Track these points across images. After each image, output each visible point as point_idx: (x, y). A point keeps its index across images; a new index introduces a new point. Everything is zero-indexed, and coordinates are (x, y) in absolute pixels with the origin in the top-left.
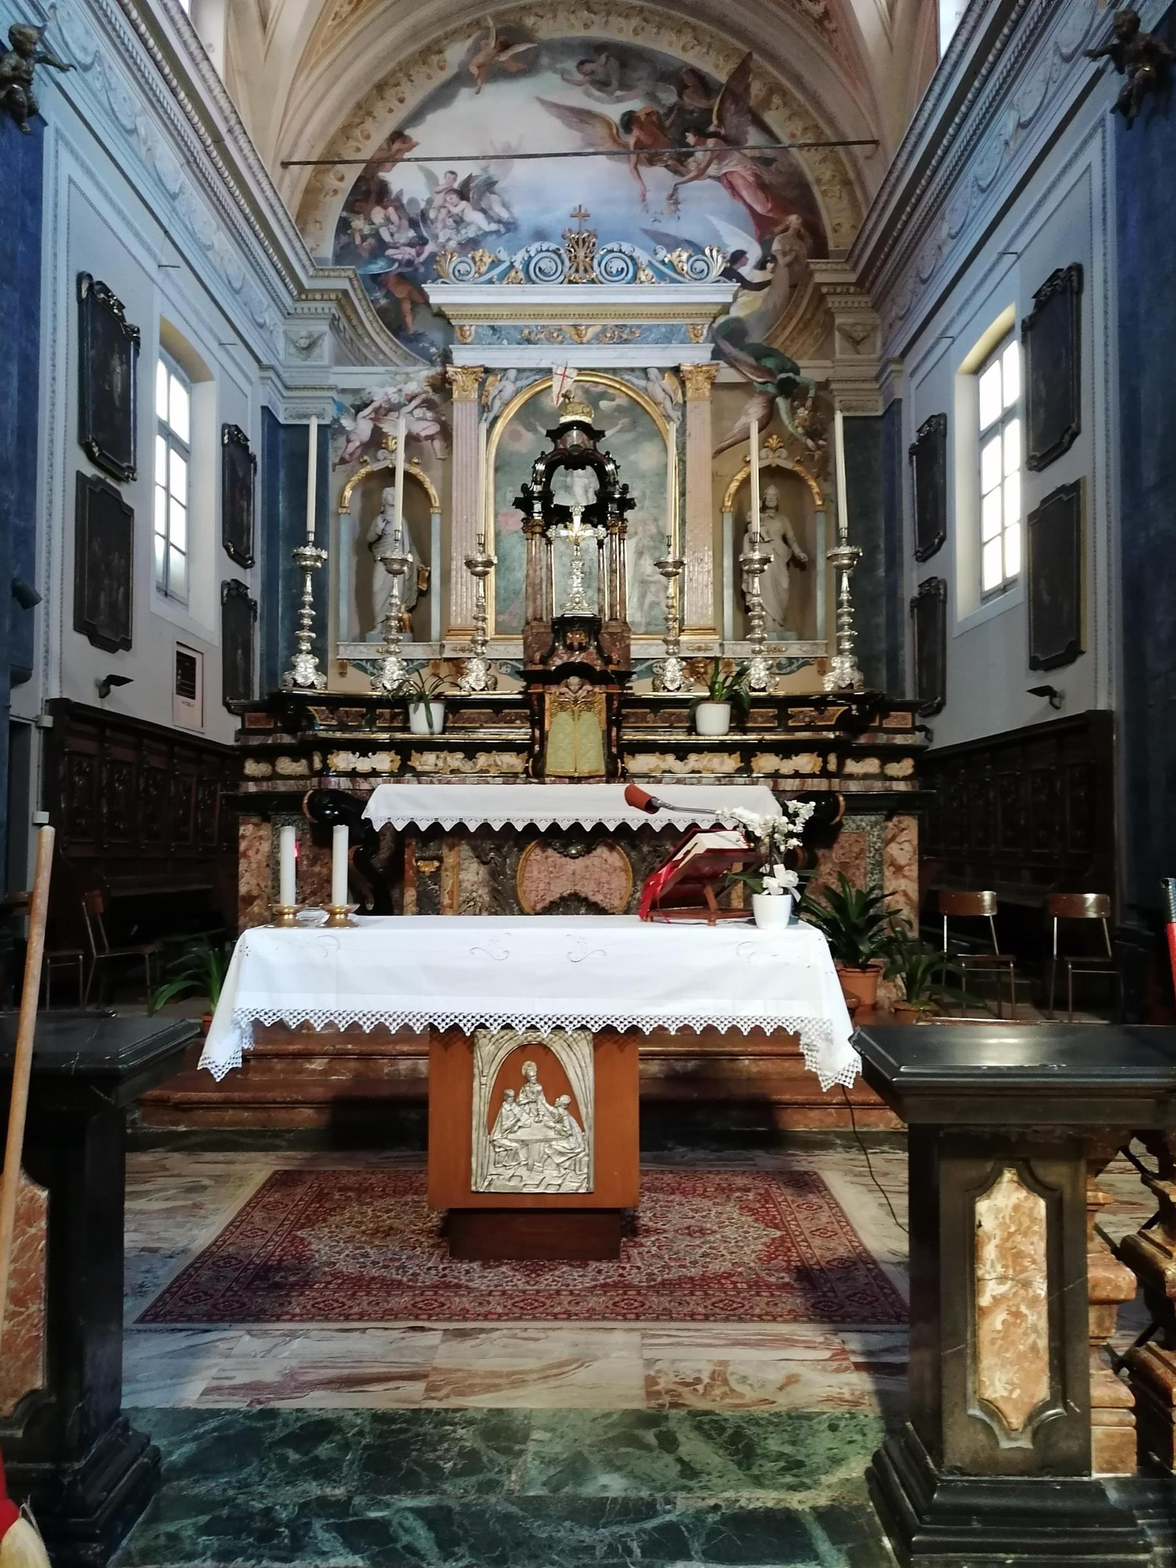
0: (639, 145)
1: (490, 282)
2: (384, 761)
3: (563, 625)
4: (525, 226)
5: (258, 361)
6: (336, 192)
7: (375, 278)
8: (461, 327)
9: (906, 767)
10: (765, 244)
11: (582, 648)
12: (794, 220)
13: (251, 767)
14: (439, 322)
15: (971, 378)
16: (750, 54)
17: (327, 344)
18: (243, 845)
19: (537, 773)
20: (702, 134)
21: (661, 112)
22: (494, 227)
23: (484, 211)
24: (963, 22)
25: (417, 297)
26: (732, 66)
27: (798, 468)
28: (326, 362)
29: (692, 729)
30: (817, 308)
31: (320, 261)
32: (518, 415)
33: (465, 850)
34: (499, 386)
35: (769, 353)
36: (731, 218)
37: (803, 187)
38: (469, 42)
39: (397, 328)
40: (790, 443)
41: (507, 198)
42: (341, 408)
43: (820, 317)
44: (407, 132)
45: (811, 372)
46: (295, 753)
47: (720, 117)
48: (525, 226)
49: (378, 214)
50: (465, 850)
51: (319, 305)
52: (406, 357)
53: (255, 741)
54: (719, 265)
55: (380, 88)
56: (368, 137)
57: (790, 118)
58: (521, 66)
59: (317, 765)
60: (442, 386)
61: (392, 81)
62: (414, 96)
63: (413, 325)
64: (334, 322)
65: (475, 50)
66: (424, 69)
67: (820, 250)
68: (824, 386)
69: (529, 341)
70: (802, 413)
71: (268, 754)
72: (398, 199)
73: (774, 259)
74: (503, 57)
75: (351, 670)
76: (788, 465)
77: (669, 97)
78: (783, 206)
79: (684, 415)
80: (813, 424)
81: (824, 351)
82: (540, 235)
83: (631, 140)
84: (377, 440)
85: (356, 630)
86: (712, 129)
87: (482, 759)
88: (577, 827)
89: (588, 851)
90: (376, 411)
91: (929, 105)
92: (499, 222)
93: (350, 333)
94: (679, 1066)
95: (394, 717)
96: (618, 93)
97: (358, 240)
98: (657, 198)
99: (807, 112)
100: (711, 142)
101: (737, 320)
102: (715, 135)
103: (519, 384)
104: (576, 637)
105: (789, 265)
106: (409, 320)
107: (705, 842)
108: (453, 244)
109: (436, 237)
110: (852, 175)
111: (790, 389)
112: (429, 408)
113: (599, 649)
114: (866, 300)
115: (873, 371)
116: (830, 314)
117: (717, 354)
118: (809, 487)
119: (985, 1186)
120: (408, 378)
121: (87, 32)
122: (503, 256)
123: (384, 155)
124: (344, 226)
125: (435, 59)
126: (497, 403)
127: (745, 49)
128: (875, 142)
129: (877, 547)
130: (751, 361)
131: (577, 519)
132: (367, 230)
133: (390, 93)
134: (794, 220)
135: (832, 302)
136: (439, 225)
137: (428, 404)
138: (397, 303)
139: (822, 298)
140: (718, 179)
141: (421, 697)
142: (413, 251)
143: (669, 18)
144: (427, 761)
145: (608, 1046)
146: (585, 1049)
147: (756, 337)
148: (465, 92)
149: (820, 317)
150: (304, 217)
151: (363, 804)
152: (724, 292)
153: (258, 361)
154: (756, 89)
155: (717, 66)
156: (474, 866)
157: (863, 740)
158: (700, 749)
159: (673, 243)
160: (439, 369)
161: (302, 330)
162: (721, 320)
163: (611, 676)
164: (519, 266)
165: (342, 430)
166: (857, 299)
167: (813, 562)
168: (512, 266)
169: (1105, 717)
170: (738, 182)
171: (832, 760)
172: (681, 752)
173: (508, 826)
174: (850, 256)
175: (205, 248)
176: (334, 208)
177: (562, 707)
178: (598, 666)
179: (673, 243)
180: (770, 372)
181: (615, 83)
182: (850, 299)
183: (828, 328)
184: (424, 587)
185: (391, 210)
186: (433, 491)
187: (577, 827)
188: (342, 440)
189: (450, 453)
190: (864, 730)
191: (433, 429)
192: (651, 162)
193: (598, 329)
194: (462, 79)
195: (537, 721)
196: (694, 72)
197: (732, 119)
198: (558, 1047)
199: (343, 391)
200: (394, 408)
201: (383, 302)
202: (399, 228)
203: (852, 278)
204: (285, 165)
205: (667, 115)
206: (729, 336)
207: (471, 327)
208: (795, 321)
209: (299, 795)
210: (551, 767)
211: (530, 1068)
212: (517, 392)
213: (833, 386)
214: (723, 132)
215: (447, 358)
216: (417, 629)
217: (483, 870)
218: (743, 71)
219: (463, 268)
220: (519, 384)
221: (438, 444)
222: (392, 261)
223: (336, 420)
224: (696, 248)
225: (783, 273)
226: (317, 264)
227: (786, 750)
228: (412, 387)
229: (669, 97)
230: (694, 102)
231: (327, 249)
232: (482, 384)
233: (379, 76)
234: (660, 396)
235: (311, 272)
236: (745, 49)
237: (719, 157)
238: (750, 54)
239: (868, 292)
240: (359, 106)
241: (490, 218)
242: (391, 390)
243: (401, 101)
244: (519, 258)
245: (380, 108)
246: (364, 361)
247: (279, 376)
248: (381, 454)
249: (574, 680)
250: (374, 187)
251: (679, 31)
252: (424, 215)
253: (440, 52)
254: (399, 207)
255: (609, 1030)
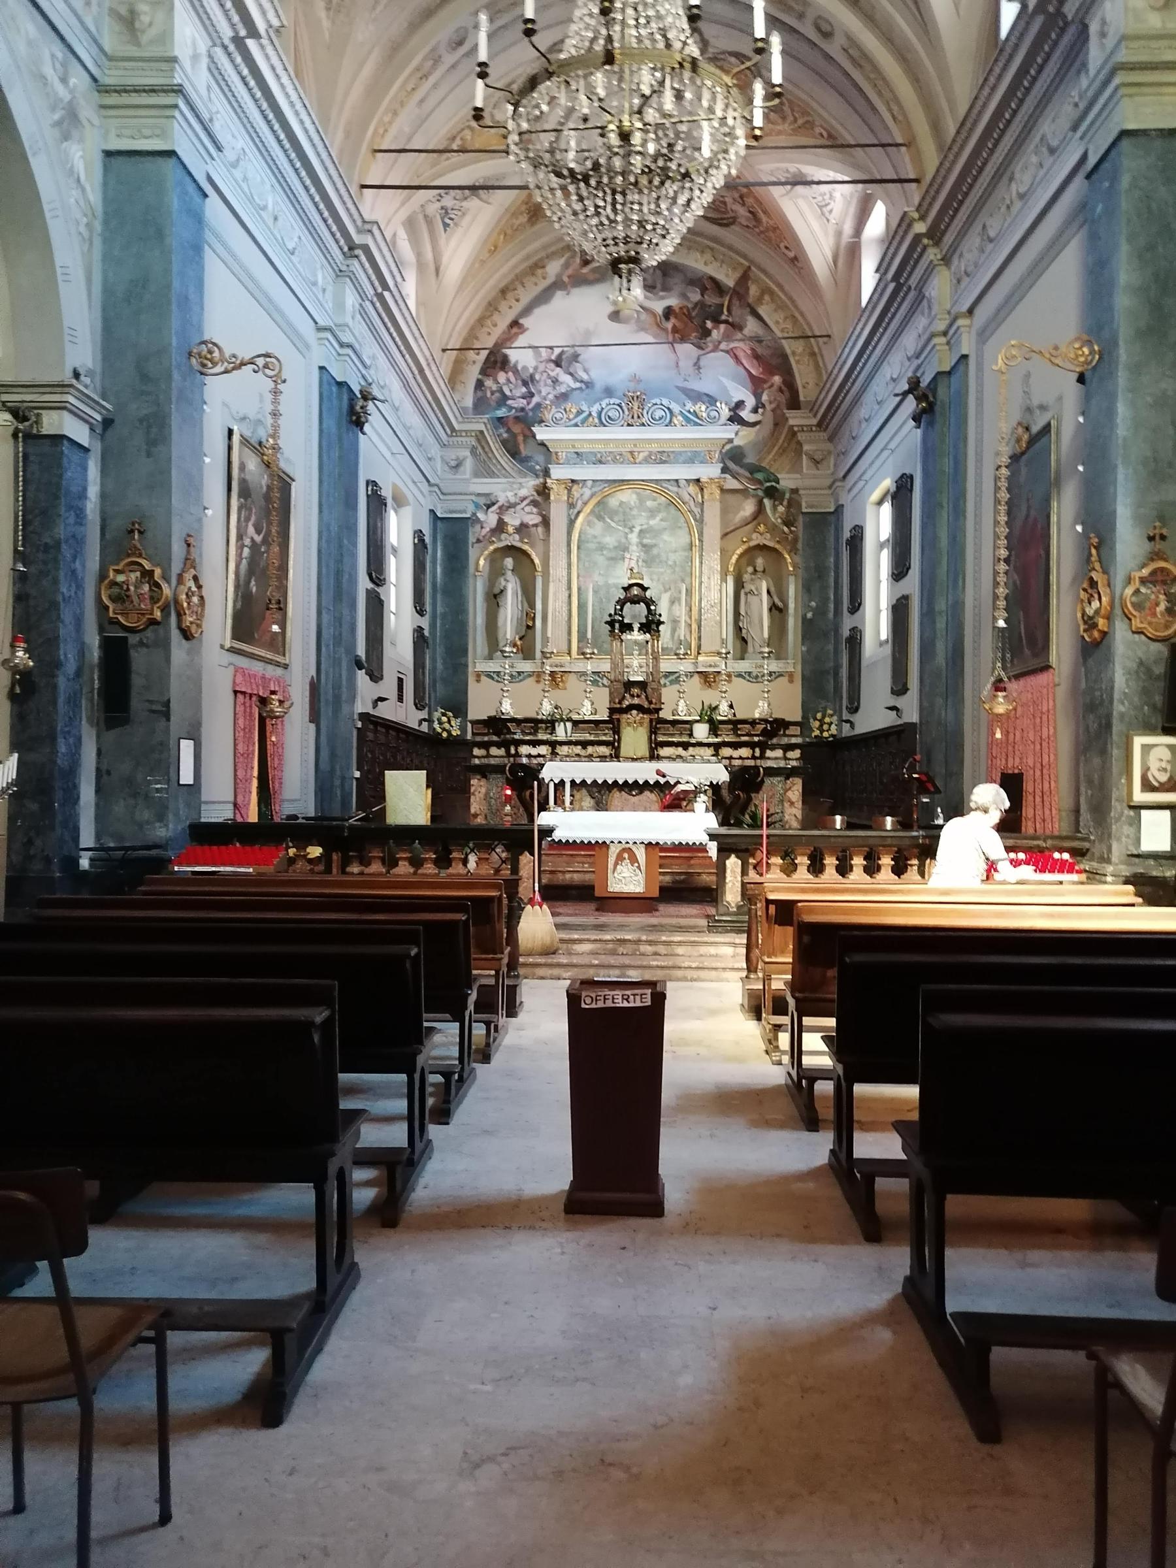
0: (675, 330)
1: (576, 425)
2: (543, 750)
3: (629, 685)
4: (599, 386)
5: (428, 481)
6: (474, 362)
7: (500, 419)
8: (556, 453)
9: (797, 753)
10: (757, 395)
11: (638, 696)
12: (777, 379)
13: (476, 751)
14: (541, 448)
15: (875, 507)
16: (749, 268)
17: (469, 464)
18: (472, 789)
19: (616, 756)
20: (717, 321)
21: (690, 306)
22: (578, 385)
23: (571, 374)
24: (875, 290)
25: (528, 433)
26: (737, 275)
27: (777, 546)
28: (468, 476)
29: (691, 735)
30: (791, 440)
31: (465, 409)
32: (592, 511)
33: (584, 791)
34: (581, 491)
35: (759, 469)
36: (735, 379)
37: (784, 357)
38: (562, 261)
39: (514, 453)
40: (772, 529)
41: (587, 366)
42: (477, 506)
43: (793, 445)
44: (521, 321)
45: (787, 481)
46: (498, 745)
47: (729, 310)
48: (599, 386)
49: (502, 377)
50: (584, 791)
51: (463, 439)
52: (520, 472)
53: (478, 739)
54: (725, 412)
55: (504, 292)
56: (495, 325)
57: (775, 310)
58: (597, 276)
59: (513, 751)
60: (543, 491)
61: (511, 287)
62: (526, 297)
63: (524, 451)
64: (473, 451)
65: (566, 266)
66: (533, 279)
67: (794, 403)
68: (795, 491)
69: (601, 462)
70: (781, 509)
71: (486, 746)
72: (515, 366)
73: (763, 406)
74: (585, 270)
75: (483, 678)
76: (771, 544)
77: (695, 296)
78: (770, 370)
79: (702, 511)
80: (787, 516)
81: (796, 468)
82: (609, 392)
83: (669, 325)
84: (501, 527)
85: (486, 652)
86: (723, 317)
87: (590, 749)
88: (636, 782)
89: (641, 793)
90: (500, 508)
91: (847, 350)
92: (582, 382)
93: (483, 456)
94: (677, 878)
95: (547, 728)
96: (661, 294)
97: (489, 394)
98: (686, 365)
99: (787, 306)
100: (722, 327)
101: (739, 447)
102: (726, 322)
103: (594, 490)
104: (636, 691)
105: (773, 410)
106: (522, 447)
107: (680, 788)
108: (551, 397)
109: (540, 392)
110: (816, 350)
111: (773, 493)
112: (535, 506)
113: (647, 697)
114: (824, 435)
115: (828, 482)
116: (800, 444)
117: (725, 470)
118: (785, 559)
119: (728, 858)
120: (521, 486)
121: (233, 136)
122: (585, 408)
123: (505, 336)
124: (479, 385)
125: (539, 271)
126: (580, 503)
127: (747, 264)
128: (829, 336)
129: (828, 598)
130: (747, 474)
131: (636, 629)
132: (494, 387)
133: (510, 295)
134: (777, 379)
135: (801, 437)
136: (542, 383)
137: (534, 503)
138: (514, 436)
139: (794, 434)
140: (727, 352)
141: (562, 720)
142: (525, 401)
143: (695, 242)
144: (564, 750)
145: (650, 849)
146: (642, 849)
147: (750, 459)
148: (559, 294)
149: (793, 445)
150: (453, 381)
151: (539, 771)
152: (729, 432)
153: (428, 481)
154: (753, 290)
155: (727, 275)
156: (588, 799)
157: (775, 741)
158: (694, 745)
159: (697, 397)
160: (541, 480)
161: (452, 455)
162: (728, 447)
163: (651, 710)
164: (594, 414)
165: (478, 520)
166: (817, 434)
167: (786, 606)
168: (590, 414)
169: (914, 724)
170: (741, 355)
171: (757, 751)
172: (685, 746)
173: (595, 782)
174: (812, 407)
175: (407, 428)
176: (473, 373)
177: (629, 724)
178: (646, 705)
179: (697, 397)
180: (760, 482)
181: (659, 286)
182: (812, 434)
183: (799, 451)
184: (530, 624)
185: (510, 374)
186: (537, 561)
187: (636, 782)
188: (478, 527)
189: (548, 535)
190: (776, 735)
191: (537, 519)
192: (683, 340)
193: (646, 454)
194: (558, 285)
195: (617, 731)
196: (713, 280)
197: (736, 311)
198: (634, 849)
199: (479, 495)
200: (512, 506)
201: (505, 435)
202: (516, 386)
203: (815, 421)
204: (444, 350)
205: (694, 309)
206: (733, 458)
207: (562, 456)
208: (776, 448)
209: (505, 766)
210: (623, 753)
211: (626, 855)
212: (592, 496)
213: (801, 492)
214: (730, 320)
215: (546, 473)
216: (526, 650)
217: (592, 801)
218: (744, 278)
219: (558, 416)
220: (594, 490)
221: (540, 529)
222: (511, 408)
223: (474, 514)
224: (711, 400)
225: (769, 414)
226: (463, 411)
227: (735, 746)
228: (524, 492)
229: (695, 296)
230: (711, 299)
231: (469, 402)
232: (569, 490)
233: (502, 285)
234: (687, 498)
235: (460, 419)
236: (747, 264)
237: (727, 337)
238: (749, 268)
239: (825, 430)
240: (490, 304)
241: (576, 380)
242: (510, 494)
243: (517, 300)
244: (595, 410)
245: (503, 306)
246: (492, 474)
247: (335, 336)
248: (503, 536)
249: (634, 712)
250: (499, 359)
251: (703, 252)
252: (532, 377)
253: (544, 267)
254: (516, 371)
255: (650, 843)
